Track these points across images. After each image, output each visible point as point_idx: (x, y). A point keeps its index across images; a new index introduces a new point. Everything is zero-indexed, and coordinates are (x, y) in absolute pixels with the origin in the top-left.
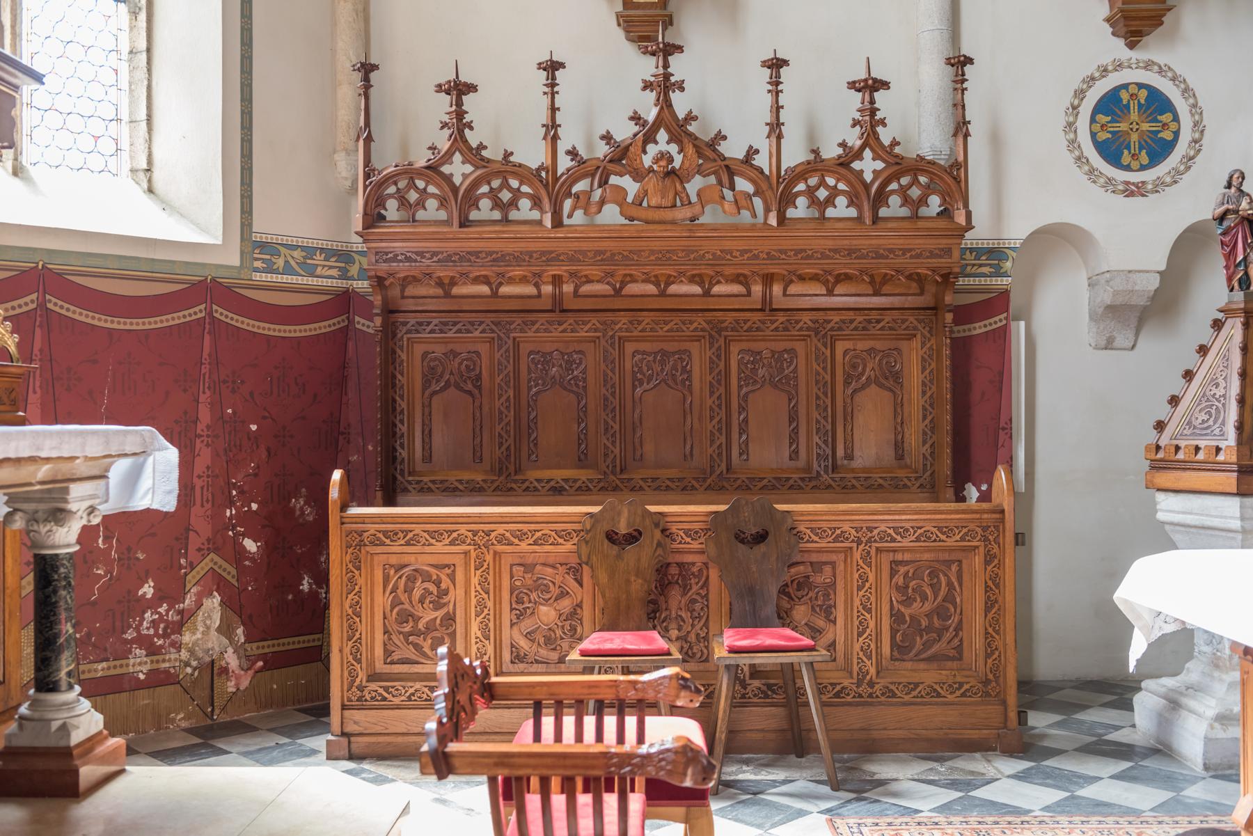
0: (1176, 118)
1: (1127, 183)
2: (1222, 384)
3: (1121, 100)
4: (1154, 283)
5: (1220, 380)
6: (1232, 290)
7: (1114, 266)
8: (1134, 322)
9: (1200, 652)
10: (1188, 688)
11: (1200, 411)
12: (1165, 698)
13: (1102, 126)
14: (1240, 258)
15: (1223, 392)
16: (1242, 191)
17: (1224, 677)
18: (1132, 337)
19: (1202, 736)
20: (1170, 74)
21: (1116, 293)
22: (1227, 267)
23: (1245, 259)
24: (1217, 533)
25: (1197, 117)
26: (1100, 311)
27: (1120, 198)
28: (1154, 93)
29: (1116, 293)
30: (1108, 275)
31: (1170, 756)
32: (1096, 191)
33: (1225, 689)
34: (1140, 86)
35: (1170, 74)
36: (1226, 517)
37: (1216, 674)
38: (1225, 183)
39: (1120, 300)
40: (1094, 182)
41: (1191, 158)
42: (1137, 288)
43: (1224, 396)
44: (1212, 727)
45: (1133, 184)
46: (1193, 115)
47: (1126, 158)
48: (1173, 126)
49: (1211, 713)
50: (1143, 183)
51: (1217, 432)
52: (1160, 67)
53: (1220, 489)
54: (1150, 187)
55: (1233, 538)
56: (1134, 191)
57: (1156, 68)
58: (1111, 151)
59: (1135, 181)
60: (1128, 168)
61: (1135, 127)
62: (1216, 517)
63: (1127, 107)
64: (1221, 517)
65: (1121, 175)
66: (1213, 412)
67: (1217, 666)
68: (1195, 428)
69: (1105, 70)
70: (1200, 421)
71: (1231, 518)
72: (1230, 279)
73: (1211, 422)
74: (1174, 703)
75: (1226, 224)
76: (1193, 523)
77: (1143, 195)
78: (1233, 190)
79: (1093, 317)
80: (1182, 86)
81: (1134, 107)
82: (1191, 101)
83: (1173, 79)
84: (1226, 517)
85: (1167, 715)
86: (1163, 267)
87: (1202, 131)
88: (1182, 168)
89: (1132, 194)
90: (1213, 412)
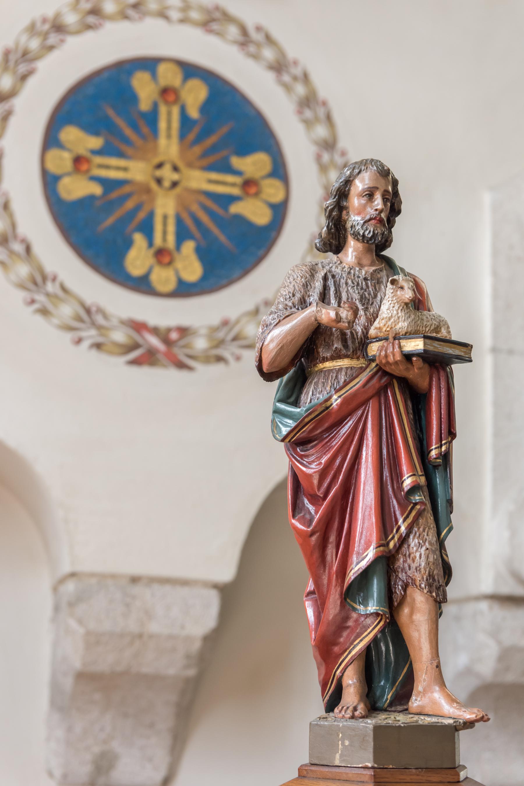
0: (279, 171)
1: (139, 327)
3: (134, 98)
4: (204, 614)
6: (333, 702)
7: (89, 564)
8: (164, 717)
13: (78, 160)
14: (364, 556)
16: (389, 263)
20: (268, 54)
21: (93, 640)
22: (320, 598)
23: (387, 562)
26: (68, 683)
27: (116, 369)
28: (224, 97)
32: (48, 337)
34: (190, 70)
35: (268, 54)
39: (106, 661)
40: (44, 312)
42: (154, 627)
45: (155, 331)
47: (138, 258)
48: (273, 191)
50: (183, 331)
52: (244, 31)
54: (200, 344)
56: (156, 350)
57: (233, 31)
58: (99, 232)
60: (142, 285)
61: (168, 175)
63: (152, 118)
65: (121, 304)
69: (95, 11)
72: (327, 649)
75: (313, 396)
77: (181, 366)
78: (352, 251)
79: (62, 704)
80: (300, 89)
81: (169, 120)
82: (321, 131)
83: (279, 67)
86: (226, 573)
89: (149, 358)
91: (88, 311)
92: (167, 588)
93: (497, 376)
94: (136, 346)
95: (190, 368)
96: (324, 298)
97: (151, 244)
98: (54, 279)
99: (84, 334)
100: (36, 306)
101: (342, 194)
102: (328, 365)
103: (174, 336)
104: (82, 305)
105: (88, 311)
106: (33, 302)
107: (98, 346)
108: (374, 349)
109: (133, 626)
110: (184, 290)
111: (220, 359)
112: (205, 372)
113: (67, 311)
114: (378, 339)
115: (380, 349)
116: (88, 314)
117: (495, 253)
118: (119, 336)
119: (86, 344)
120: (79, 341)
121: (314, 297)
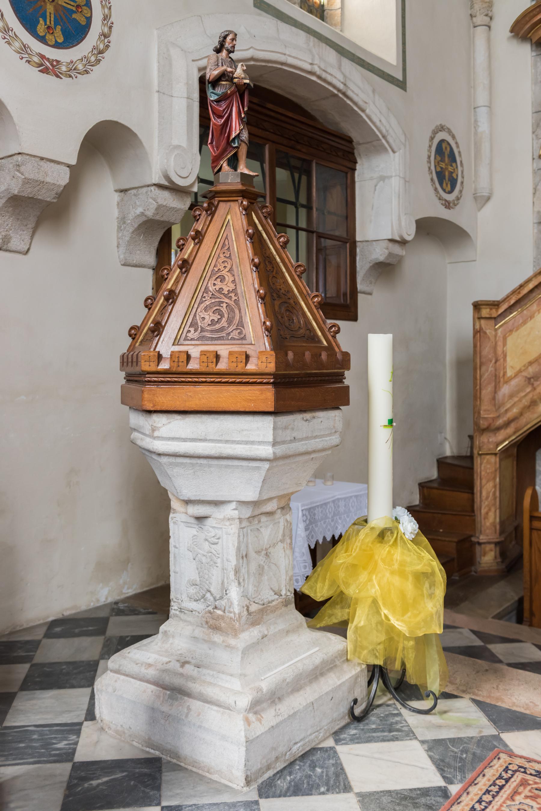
1: (42, 57)
2: (229, 278)
5: (224, 273)
8: (31, 225)
9: (181, 610)
10: (183, 664)
11: (206, 309)
12: (156, 683)
15: (232, 286)
17: (232, 642)
18: (27, 238)
19: (243, 740)
24: (236, 463)
25: (106, 11)
29: (27, 182)
30: (19, 158)
31: (202, 778)
33: (239, 659)
36: (252, 443)
37: (217, 638)
38: (216, 44)
39: (27, 192)
40: (9, 43)
41: (101, 52)
42: (48, 180)
43: (234, 291)
44: (248, 721)
45: (48, 59)
46: (103, 7)
49: (244, 702)
50: (58, 62)
51: (235, 335)
53: (252, 407)
55: (258, 468)
56: (49, 68)
59: (51, 57)
62: (238, 442)
64: (247, 443)
66: (224, 310)
67: (216, 628)
68: (203, 330)
70: (208, 320)
71: (260, 443)
73: (224, 323)
74: (173, 690)
76: (206, 452)
77: (58, 76)
78: (224, 53)
84: (252, 443)
85: (165, 708)
87: (110, 28)
88: (93, 59)
89: (45, 71)
90: (224, 310)
91: (25, 46)
92: (52, 164)
93: (159, 102)
94: (41, 65)
95: (61, 78)
96: (222, 65)
97: (46, 24)
98: (12, 30)
99: (24, 56)
100: (6, 40)
101: (225, 37)
102: (223, 83)
103: (55, 63)
104: (23, 43)
105: (25, 46)
106: (5, 38)
107: (29, 62)
108: (236, 80)
109: (41, 179)
110: (57, 46)
111: (70, 76)
112: (66, 80)
113: (17, 44)
114: (236, 78)
115: (238, 81)
116: (25, 48)
117: (159, 54)
118: (36, 59)
119: (25, 60)
120: (22, 58)
121: (220, 64)
